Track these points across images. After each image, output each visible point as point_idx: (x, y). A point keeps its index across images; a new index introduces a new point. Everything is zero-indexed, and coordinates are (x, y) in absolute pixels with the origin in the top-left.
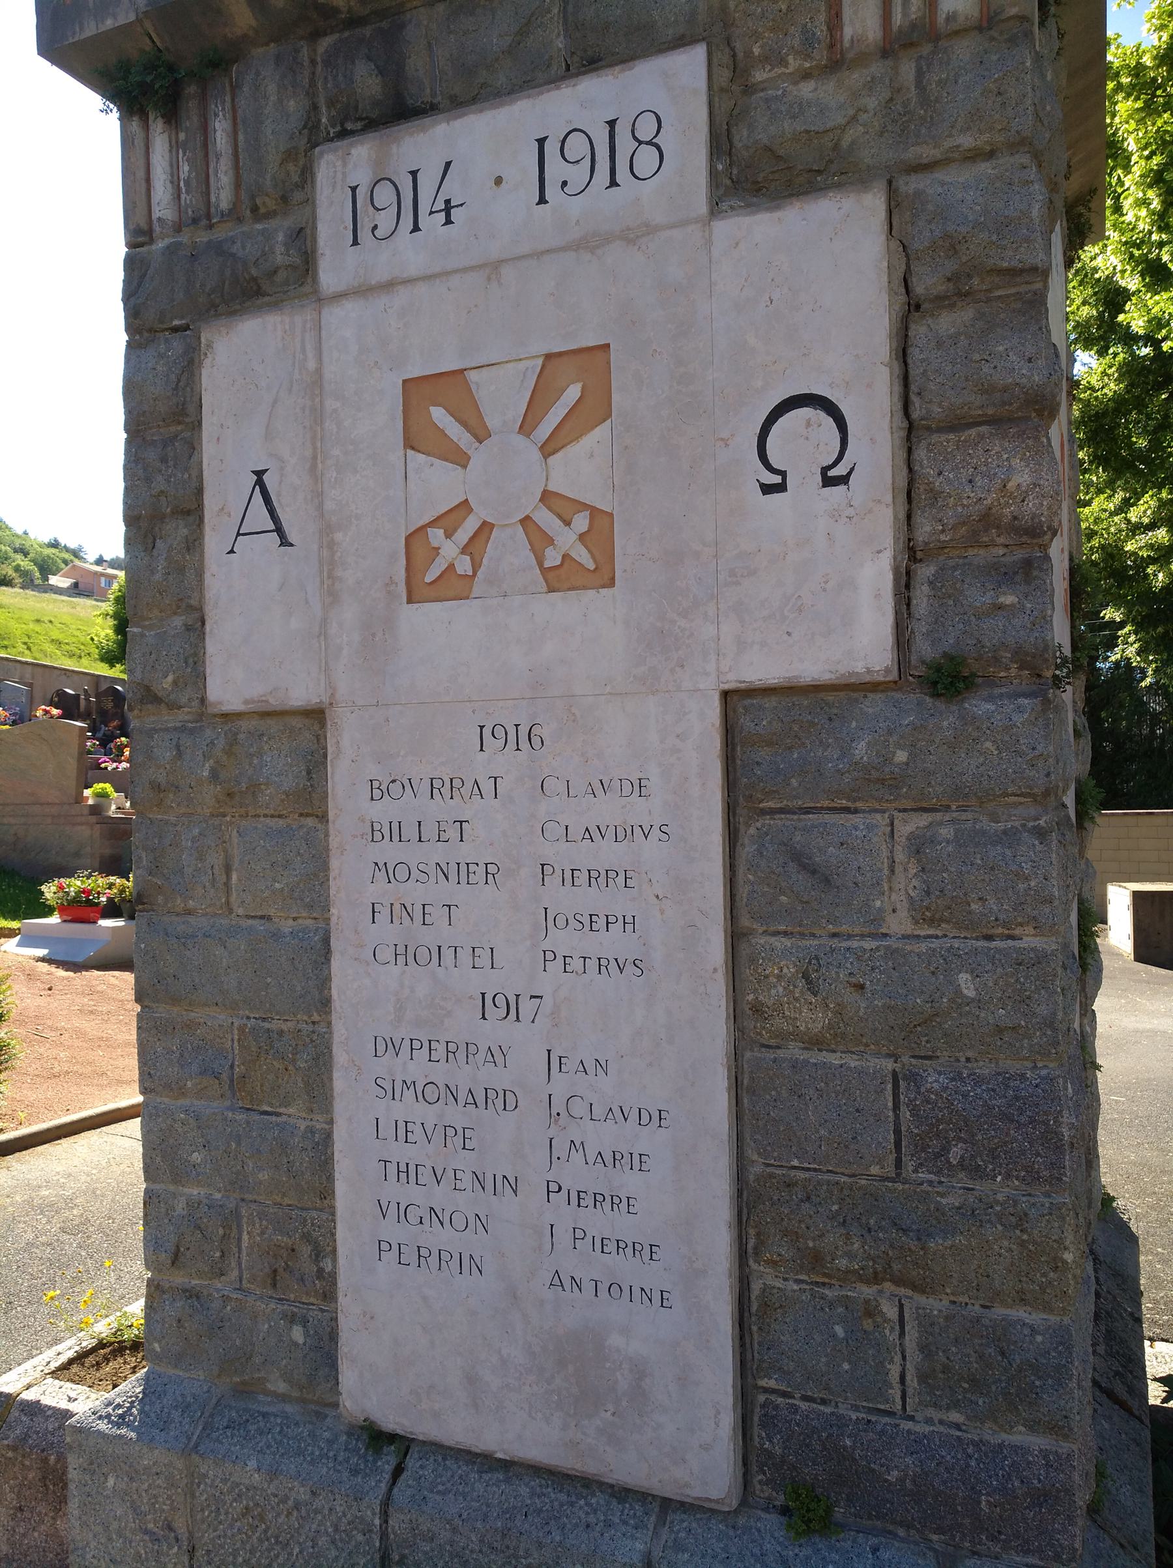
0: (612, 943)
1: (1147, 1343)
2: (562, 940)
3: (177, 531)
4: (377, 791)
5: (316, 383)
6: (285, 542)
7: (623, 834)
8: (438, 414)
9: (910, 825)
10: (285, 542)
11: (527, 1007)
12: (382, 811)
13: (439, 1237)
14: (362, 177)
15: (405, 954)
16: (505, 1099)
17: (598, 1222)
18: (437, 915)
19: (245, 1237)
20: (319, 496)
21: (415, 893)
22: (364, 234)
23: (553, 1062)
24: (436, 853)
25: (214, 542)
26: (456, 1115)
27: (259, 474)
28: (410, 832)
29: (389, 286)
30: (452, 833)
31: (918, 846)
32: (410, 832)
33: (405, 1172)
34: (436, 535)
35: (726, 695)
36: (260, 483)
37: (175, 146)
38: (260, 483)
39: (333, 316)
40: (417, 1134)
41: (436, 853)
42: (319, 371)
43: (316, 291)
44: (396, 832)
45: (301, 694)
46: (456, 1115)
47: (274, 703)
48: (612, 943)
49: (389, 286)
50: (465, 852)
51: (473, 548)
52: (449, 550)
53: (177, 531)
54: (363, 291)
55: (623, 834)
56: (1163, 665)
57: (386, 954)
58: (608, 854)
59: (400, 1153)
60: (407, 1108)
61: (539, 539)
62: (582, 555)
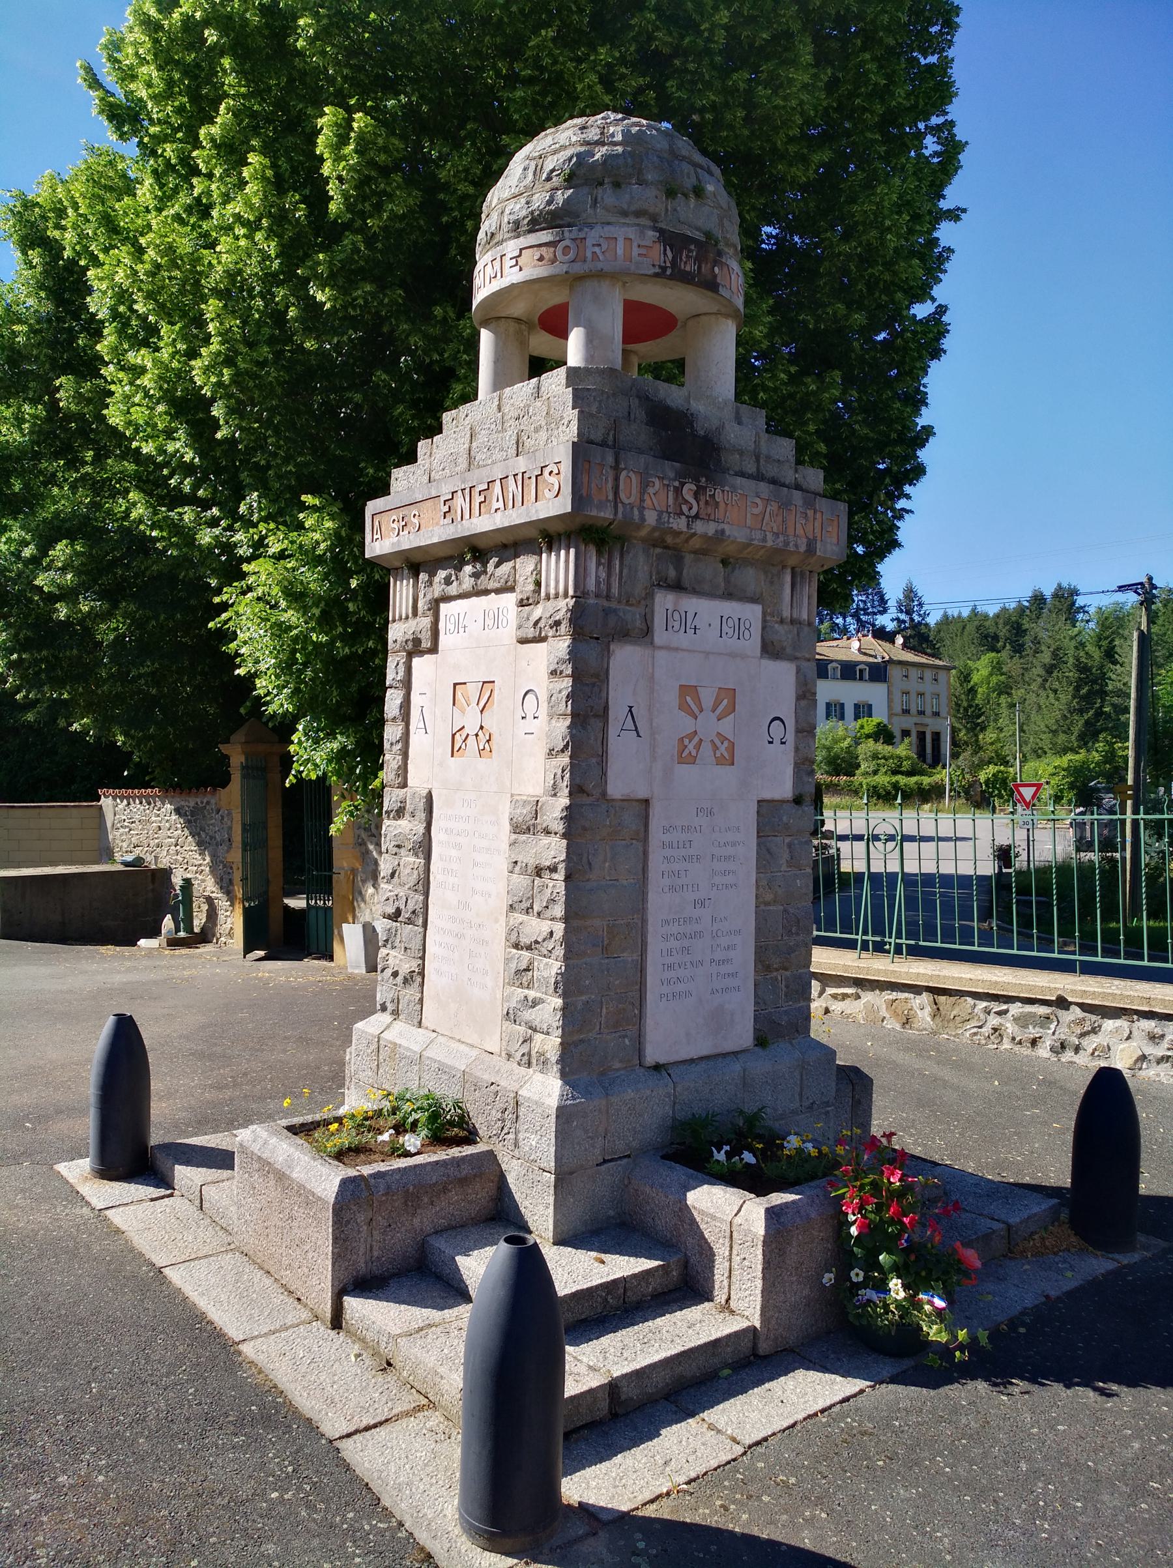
0: (730, 879)
1: (815, 985)
2: (718, 880)
3: (597, 724)
4: (666, 830)
5: (652, 678)
6: (639, 736)
7: (734, 844)
8: (688, 699)
9: (788, 840)
10: (639, 736)
11: (707, 902)
12: (666, 838)
13: (681, 987)
14: (670, 607)
15: (672, 888)
16: (698, 935)
17: (724, 969)
18: (683, 873)
19: (604, 1010)
20: (651, 721)
21: (676, 867)
22: (670, 628)
23: (714, 919)
24: (683, 852)
25: (613, 731)
26: (686, 943)
27: (631, 707)
28: (675, 845)
29: (677, 649)
30: (688, 845)
31: (790, 846)
32: (675, 845)
33: (670, 967)
34: (686, 741)
35: (759, 802)
36: (630, 711)
37: (598, 564)
38: (630, 711)
39: (660, 655)
40: (674, 952)
41: (683, 852)
42: (653, 674)
43: (652, 643)
44: (671, 846)
45: (642, 794)
46: (686, 943)
47: (632, 796)
48: (730, 879)
49: (677, 649)
50: (692, 852)
51: (698, 747)
52: (691, 747)
53: (597, 724)
54: (668, 648)
55: (734, 844)
56: (193, 271)
57: (666, 890)
58: (730, 851)
59: (669, 960)
60: (673, 944)
61: (715, 748)
62: (726, 755)
